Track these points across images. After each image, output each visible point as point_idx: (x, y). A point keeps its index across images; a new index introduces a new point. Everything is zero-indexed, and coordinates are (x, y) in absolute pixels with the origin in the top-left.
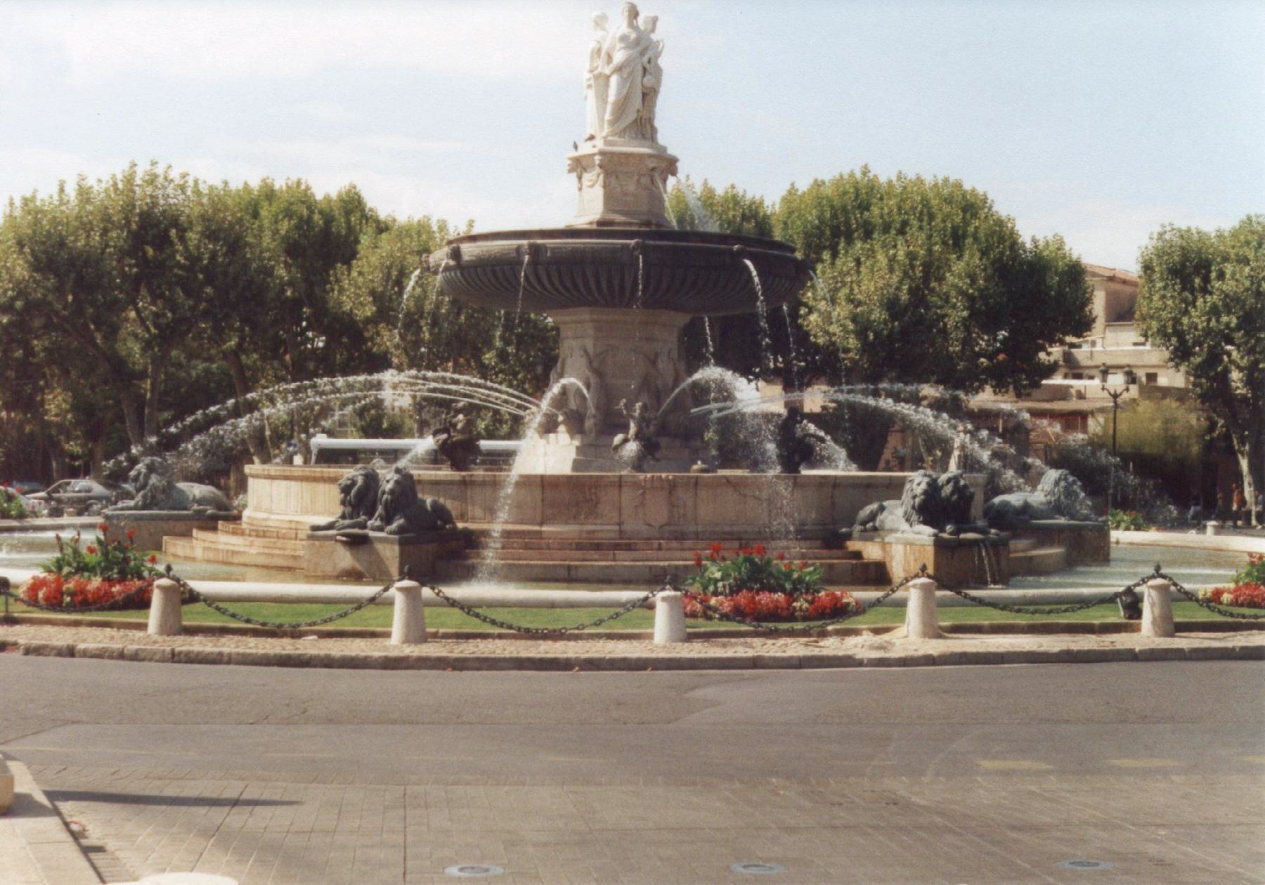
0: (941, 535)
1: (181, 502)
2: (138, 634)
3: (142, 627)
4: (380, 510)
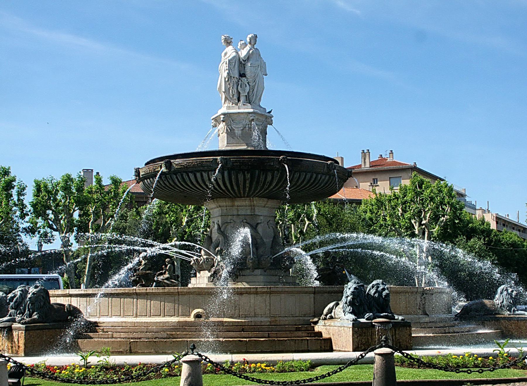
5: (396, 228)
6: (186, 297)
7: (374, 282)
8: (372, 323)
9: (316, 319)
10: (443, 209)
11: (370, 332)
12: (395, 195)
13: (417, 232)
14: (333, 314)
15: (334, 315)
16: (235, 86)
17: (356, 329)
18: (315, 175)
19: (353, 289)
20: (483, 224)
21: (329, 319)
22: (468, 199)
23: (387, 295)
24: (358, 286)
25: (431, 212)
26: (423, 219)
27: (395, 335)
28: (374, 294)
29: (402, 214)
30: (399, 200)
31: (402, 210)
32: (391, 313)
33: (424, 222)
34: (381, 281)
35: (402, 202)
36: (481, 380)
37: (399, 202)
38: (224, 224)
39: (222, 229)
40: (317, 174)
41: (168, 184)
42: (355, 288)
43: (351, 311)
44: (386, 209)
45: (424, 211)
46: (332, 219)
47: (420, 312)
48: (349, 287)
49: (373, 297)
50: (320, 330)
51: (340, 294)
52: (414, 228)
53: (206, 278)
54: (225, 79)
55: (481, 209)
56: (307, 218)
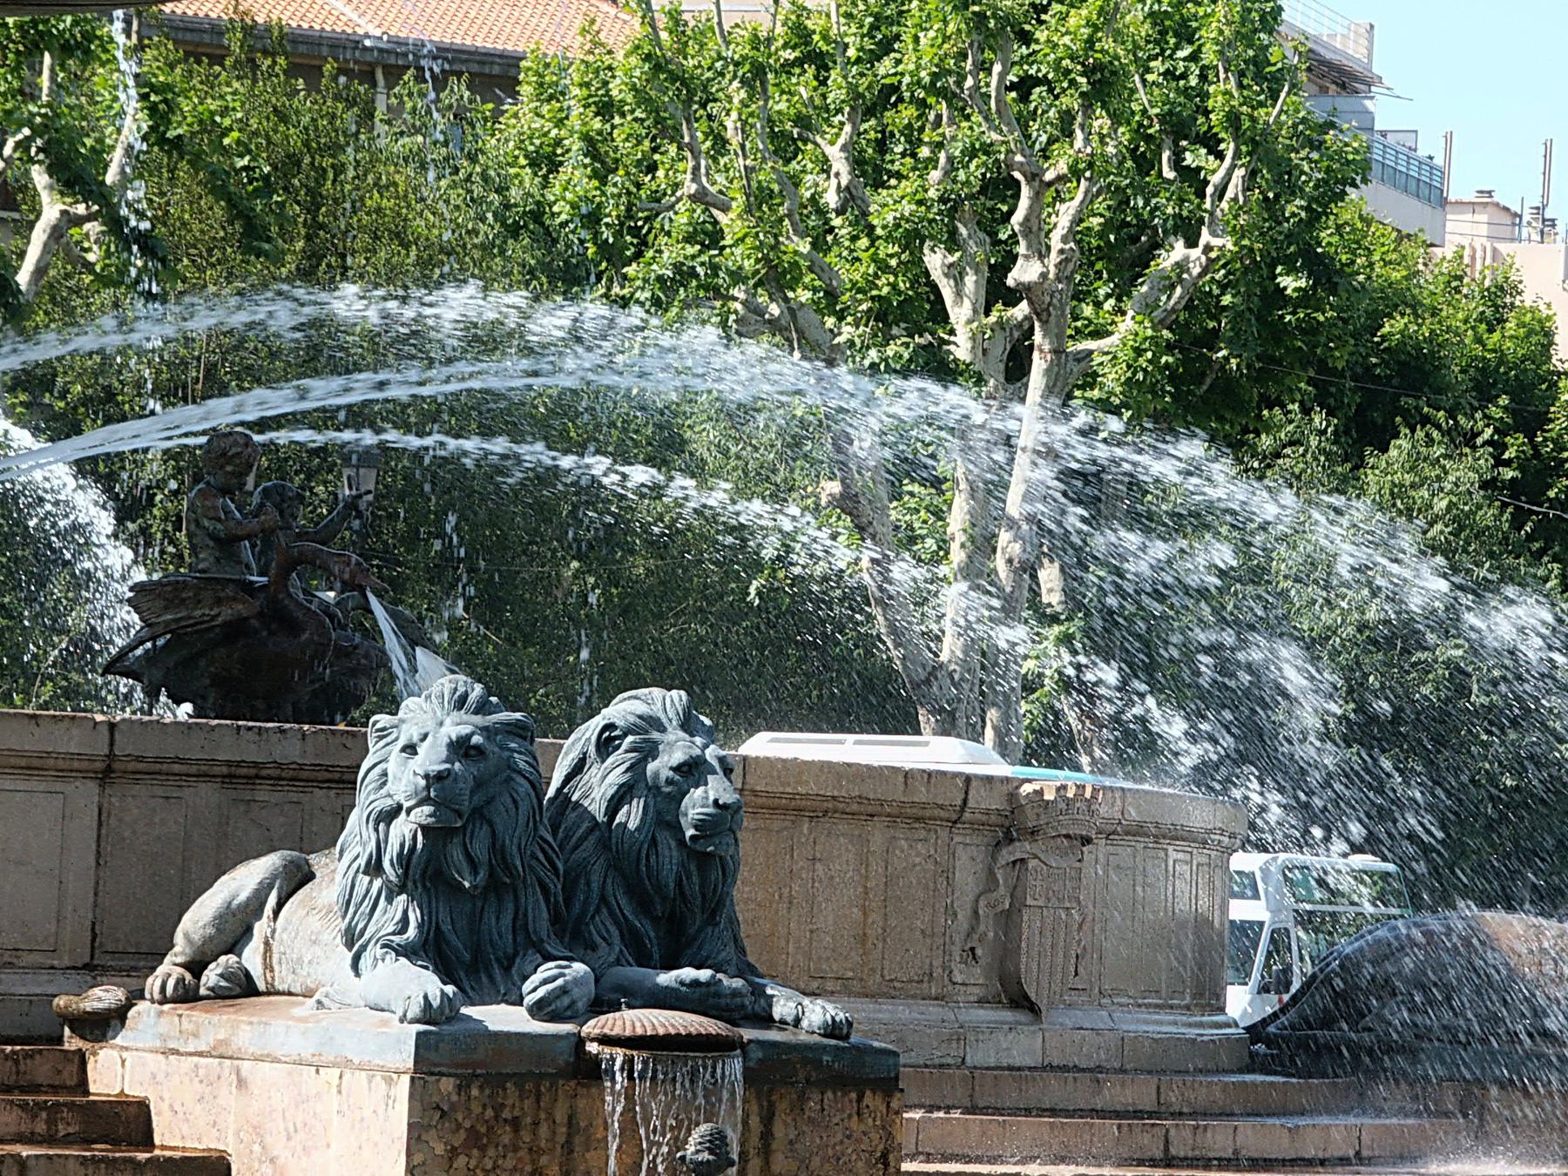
5: (792, 311)
7: (623, 709)
8: (580, 1041)
9: (103, 996)
10: (1193, 178)
11: (560, 1115)
12: (800, 34)
13: (961, 349)
14: (251, 958)
15: (268, 966)
17: (447, 1085)
19: (443, 753)
20: (1495, 322)
21: (218, 995)
22: (1385, 112)
23: (722, 820)
24: (485, 730)
25: (1090, 199)
26: (1022, 249)
27: (766, 1152)
28: (615, 804)
29: (850, 199)
30: (835, 75)
31: (858, 163)
32: (746, 970)
33: (1025, 272)
34: (678, 696)
35: (855, 94)
37: (836, 94)
42: (460, 748)
43: (412, 932)
44: (720, 143)
45: (1034, 177)
46: (267, 187)
47: (973, 977)
48: (409, 733)
49: (604, 832)
50: (134, 1091)
51: (322, 797)
52: (940, 315)
55: (1485, 201)
56: (51, 171)
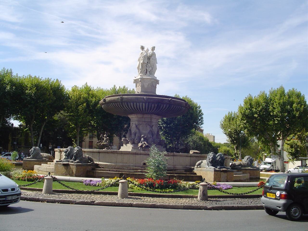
0: (216, 169)
1: (42, 157)
2: (39, 193)
3: (116, 194)
4: (73, 158)
6: (139, 156)
16: (146, 67)
18: (181, 107)
36: (34, 189)
38: (139, 124)
39: (138, 127)
40: (182, 107)
41: (120, 107)
42: (213, 156)
53: (131, 147)
54: (141, 64)
